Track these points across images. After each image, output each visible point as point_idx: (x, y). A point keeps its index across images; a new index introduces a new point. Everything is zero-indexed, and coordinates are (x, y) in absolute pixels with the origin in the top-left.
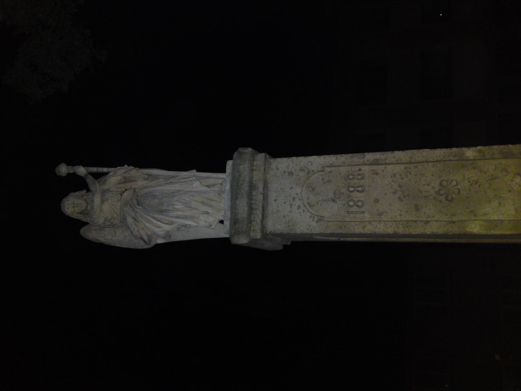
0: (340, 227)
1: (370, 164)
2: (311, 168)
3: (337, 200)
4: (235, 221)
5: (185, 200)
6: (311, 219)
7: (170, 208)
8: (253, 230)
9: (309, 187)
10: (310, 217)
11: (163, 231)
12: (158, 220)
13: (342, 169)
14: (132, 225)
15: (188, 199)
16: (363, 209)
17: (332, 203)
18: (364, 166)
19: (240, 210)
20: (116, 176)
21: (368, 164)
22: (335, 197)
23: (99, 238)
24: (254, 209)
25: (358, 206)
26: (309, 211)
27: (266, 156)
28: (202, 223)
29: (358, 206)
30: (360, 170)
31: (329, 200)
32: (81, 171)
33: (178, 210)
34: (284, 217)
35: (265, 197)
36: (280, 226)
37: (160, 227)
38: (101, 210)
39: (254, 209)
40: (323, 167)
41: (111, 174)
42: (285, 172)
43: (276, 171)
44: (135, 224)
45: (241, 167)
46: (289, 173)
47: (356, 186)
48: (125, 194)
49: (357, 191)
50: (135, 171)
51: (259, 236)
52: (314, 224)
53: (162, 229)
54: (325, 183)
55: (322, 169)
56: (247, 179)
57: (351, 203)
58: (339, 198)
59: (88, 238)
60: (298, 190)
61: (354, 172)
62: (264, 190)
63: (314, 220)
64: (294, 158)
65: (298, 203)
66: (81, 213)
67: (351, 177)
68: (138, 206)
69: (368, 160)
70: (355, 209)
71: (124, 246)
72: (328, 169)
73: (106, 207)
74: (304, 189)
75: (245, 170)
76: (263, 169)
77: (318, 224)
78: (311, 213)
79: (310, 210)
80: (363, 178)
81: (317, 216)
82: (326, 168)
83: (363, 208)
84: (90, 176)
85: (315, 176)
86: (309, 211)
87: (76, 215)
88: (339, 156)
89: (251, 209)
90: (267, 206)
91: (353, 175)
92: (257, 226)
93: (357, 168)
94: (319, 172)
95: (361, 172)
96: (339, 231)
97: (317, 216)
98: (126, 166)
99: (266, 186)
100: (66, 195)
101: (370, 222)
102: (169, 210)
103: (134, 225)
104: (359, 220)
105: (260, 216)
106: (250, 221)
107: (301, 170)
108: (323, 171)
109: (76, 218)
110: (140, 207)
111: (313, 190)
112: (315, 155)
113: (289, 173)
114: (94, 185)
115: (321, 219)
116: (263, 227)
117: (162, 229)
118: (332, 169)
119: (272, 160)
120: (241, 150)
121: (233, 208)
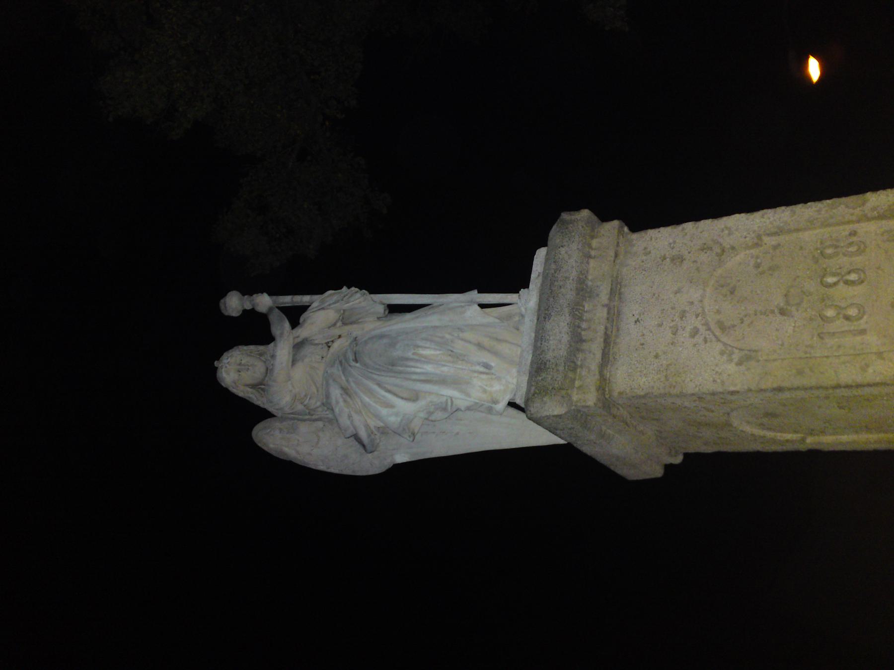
0: (800, 372)
1: (881, 217)
2: (727, 242)
3: (794, 309)
4: (538, 367)
5: (442, 338)
6: (725, 357)
7: (410, 354)
8: (580, 388)
9: (722, 286)
10: (722, 353)
11: (397, 414)
12: (389, 391)
13: (807, 236)
14: (337, 403)
15: (448, 336)
16: (862, 324)
17: (779, 318)
18: (863, 224)
19: (551, 342)
20: (325, 311)
21: (874, 218)
22: (787, 303)
23: (286, 450)
24: (584, 341)
25: (847, 318)
26: (718, 340)
27: (621, 228)
28: (476, 395)
29: (847, 318)
30: (853, 233)
31: (773, 312)
32: (263, 302)
33: (428, 360)
34: (657, 356)
35: (614, 316)
36: (644, 379)
37: (392, 406)
38: (289, 378)
39: (584, 341)
40: (759, 237)
41: (315, 305)
42: (664, 258)
43: (644, 258)
44: (345, 401)
45: (563, 250)
46: (673, 260)
47: (845, 270)
48: (336, 345)
49: (847, 282)
50: (358, 295)
51: (591, 399)
52: (732, 368)
53: (395, 410)
54: (762, 273)
55: (756, 241)
56: (574, 274)
57: (830, 313)
58: (798, 304)
59: (265, 448)
60: (695, 294)
61: (838, 241)
62: (610, 299)
63: (730, 360)
64: (689, 226)
65: (692, 322)
66: (253, 386)
67: (829, 251)
68: (353, 364)
69: (874, 209)
70: (840, 324)
71: (332, 470)
72: (774, 241)
73: (299, 372)
74: (709, 290)
75: (570, 257)
76: (612, 254)
77: (743, 368)
78: (725, 344)
79: (724, 339)
80: (860, 252)
81: (741, 350)
82: (766, 239)
83: (862, 321)
84: (277, 310)
85: (738, 258)
86: (718, 340)
87: (242, 388)
88: (799, 209)
89: (577, 340)
90: (617, 336)
91: (836, 247)
92: (589, 377)
93: (845, 230)
94: (748, 247)
95: (854, 239)
96: (798, 382)
97: (741, 350)
98: (345, 288)
99: (616, 291)
100: (229, 346)
101: (880, 355)
102: (407, 359)
103: (342, 404)
104: (852, 352)
105: (599, 355)
106: (572, 365)
107: (705, 248)
108: (757, 245)
109: (241, 394)
110: (358, 365)
111: (732, 293)
112: (740, 212)
113: (673, 260)
114: (285, 337)
115: (748, 357)
116: (603, 383)
117: (395, 410)
118: (781, 239)
119: (635, 236)
120: (565, 216)
121: (540, 336)
